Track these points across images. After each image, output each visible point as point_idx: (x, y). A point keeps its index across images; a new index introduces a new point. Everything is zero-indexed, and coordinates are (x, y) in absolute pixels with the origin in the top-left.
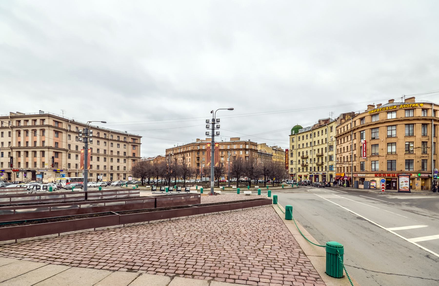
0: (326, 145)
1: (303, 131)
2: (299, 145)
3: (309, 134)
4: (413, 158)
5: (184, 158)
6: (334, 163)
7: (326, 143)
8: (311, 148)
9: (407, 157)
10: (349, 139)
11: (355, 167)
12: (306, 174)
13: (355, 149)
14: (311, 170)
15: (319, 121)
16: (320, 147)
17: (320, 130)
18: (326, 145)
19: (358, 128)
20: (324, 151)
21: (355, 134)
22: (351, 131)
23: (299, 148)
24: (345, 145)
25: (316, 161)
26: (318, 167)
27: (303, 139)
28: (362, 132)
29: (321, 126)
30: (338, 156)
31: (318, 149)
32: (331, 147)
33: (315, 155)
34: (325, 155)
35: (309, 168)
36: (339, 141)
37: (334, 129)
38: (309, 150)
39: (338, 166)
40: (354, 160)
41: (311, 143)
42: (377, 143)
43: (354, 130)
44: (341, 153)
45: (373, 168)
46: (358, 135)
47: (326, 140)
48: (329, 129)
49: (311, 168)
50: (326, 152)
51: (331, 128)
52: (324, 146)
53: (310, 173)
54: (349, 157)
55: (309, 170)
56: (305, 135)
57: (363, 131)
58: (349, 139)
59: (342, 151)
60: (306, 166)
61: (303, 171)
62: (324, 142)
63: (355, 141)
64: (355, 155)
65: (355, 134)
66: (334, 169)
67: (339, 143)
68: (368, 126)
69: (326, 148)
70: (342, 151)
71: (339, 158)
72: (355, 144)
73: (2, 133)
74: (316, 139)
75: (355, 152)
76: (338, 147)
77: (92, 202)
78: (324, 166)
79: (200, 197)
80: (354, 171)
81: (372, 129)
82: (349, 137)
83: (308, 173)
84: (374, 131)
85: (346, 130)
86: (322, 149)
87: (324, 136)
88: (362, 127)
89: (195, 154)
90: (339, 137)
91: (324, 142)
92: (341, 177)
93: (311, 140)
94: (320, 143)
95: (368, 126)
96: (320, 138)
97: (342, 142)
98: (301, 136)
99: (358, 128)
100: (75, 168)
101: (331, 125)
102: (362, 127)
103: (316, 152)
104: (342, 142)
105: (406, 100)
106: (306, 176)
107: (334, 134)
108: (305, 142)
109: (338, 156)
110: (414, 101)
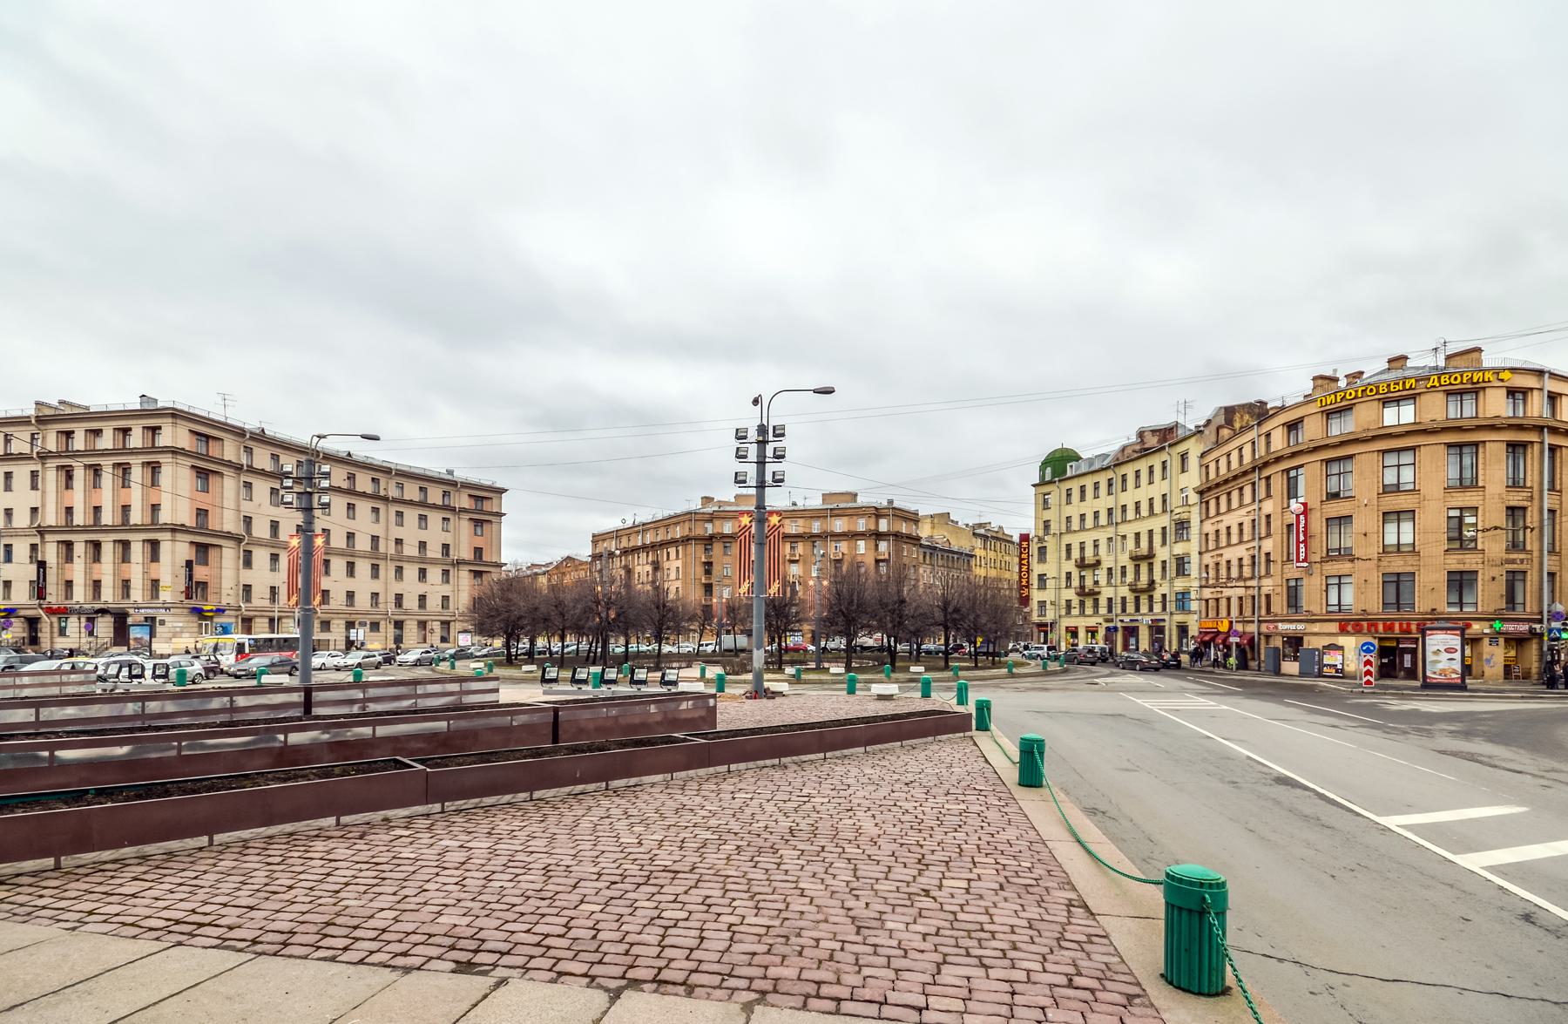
0: (1165, 521)
1: (1084, 469)
2: (1069, 519)
3: (1102, 479)
4: (1474, 567)
5: (657, 566)
6: (1192, 582)
7: (1164, 511)
8: (1110, 532)
9: (1454, 562)
10: (1247, 498)
11: (1268, 596)
12: (1092, 622)
13: (1269, 535)
14: (1110, 610)
15: (1141, 434)
16: (1143, 527)
17: (1143, 465)
18: (1165, 521)
19: (1278, 460)
20: (1157, 539)
21: (1268, 478)
22: (1254, 469)
23: (1069, 531)
24: (1232, 520)
25: (1130, 578)
26: (1137, 599)
27: (1083, 499)
28: (1293, 473)
29: (1145, 452)
30: (1207, 559)
31: (1138, 535)
32: (1182, 526)
33: (1127, 556)
34: (1162, 554)
35: (1103, 602)
36: (1212, 503)
37: (1193, 462)
38: (1102, 536)
39: (1207, 593)
40: (1263, 573)
41: (1110, 511)
42: (1346, 513)
43: (1266, 464)
44: (1218, 548)
45: (1334, 600)
46: (1278, 484)
47: (1164, 501)
48: (1176, 461)
49: (1110, 600)
50: (1164, 543)
51: (1184, 457)
52: (1157, 524)
53: (1107, 621)
54: (1246, 561)
55: (1103, 610)
56: (1088, 482)
57: (1297, 468)
58: (1247, 498)
59: (1223, 542)
60: (1094, 595)
61: (1082, 613)
62: (1158, 508)
63: (1268, 507)
64: (1268, 554)
65: (1268, 478)
66: (1194, 606)
67: (1212, 512)
68: (1316, 449)
69: (1164, 529)
70: (1223, 542)
71: (1212, 566)
72: (1268, 516)
73: (8, 475)
74: (1128, 498)
75: (1268, 545)
76: (1209, 527)
77: (329, 724)
78: (1157, 596)
79: (715, 707)
80: (1263, 612)
81: (1328, 462)
82: (1248, 490)
83: (1100, 620)
84: (1335, 471)
85: (1235, 464)
86: (1151, 532)
87: (1159, 488)
88: (1294, 455)
89: (697, 552)
90: (1209, 489)
91: (1158, 508)
92: (1219, 633)
93: (1109, 502)
94: (1144, 511)
95: (1316, 449)
96: (1142, 494)
97: (1223, 508)
98: (1075, 486)
99: (1278, 460)
100: (267, 603)
101: (1181, 448)
102: (1294, 455)
103: (1130, 544)
104: (1223, 508)
105: (1448, 358)
106: (1092, 632)
107: (1192, 479)
108: (1088, 507)
109: (1207, 559)
110: (1480, 361)
